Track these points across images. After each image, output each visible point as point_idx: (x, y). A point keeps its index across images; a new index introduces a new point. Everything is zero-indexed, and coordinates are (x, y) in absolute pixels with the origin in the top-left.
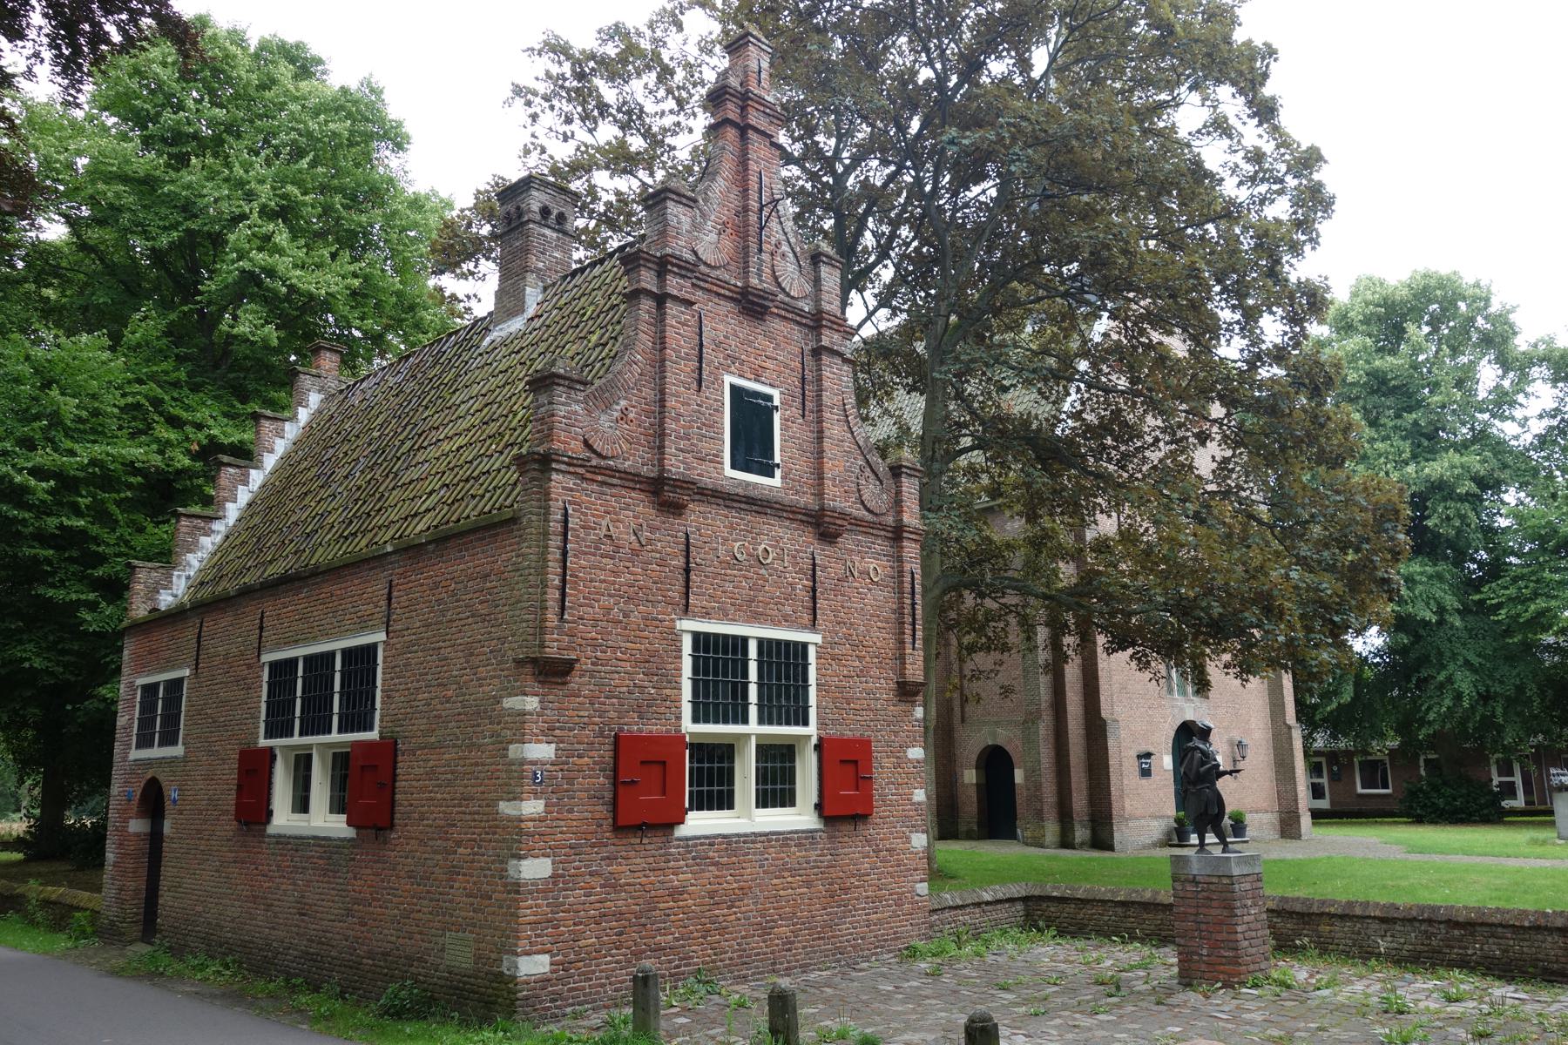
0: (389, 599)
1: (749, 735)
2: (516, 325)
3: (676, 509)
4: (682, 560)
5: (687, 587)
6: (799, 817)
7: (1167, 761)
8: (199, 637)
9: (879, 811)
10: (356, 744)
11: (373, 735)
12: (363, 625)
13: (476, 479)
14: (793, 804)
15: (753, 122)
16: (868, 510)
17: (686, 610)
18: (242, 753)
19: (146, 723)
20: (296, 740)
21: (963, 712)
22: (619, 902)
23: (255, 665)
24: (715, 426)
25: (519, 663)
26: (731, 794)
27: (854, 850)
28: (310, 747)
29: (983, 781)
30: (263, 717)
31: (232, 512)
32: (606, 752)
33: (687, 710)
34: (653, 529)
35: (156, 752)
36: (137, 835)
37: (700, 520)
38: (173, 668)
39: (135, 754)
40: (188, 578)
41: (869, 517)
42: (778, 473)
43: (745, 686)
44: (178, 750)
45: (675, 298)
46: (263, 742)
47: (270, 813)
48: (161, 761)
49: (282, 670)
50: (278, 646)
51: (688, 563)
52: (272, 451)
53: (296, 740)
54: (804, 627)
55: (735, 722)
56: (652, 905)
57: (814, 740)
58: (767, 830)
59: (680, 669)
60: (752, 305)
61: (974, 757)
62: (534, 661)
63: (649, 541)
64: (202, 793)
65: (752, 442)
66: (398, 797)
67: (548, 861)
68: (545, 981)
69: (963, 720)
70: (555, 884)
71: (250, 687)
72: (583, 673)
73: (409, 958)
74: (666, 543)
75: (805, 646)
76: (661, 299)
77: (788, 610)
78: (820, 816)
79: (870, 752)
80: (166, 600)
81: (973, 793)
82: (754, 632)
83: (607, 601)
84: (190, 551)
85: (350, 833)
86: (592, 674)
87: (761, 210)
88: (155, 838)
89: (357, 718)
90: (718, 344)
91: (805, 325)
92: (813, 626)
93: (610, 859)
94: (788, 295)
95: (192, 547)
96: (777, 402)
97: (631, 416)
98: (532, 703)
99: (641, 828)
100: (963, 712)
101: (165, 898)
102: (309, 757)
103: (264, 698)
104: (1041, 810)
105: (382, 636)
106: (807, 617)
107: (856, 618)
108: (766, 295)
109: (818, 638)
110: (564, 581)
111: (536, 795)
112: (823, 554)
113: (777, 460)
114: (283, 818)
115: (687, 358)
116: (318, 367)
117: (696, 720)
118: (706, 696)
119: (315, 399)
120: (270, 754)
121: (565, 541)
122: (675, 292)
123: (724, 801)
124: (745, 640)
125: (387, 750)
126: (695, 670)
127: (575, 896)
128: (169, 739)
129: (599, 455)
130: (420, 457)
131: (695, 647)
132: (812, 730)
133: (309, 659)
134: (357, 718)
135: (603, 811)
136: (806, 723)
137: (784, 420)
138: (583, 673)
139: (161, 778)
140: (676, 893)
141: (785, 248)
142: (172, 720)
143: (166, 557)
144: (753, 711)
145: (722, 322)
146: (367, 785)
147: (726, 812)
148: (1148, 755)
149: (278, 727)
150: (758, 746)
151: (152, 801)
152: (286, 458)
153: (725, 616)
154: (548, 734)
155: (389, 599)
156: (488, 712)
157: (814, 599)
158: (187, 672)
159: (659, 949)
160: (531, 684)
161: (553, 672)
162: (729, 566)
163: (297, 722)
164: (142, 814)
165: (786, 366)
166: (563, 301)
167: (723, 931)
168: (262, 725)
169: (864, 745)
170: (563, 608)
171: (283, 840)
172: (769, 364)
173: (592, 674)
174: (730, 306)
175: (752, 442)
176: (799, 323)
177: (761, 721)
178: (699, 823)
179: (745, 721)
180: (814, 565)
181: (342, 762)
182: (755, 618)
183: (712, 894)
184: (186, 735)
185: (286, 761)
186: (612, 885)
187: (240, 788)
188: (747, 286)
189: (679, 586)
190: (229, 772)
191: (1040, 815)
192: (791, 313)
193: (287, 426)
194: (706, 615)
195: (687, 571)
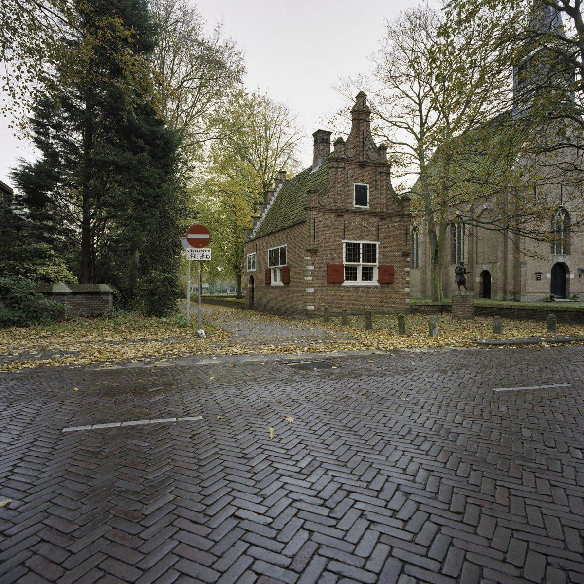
3: (342, 216)
6: (374, 282)
7: (549, 275)
11: (286, 265)
17: (344, 239)
20: (280, 266)
22: (329, 298)
26: (356, 277)
29: (482, 281)
33: (344, 260)
35: (252, 270)
42: (368, 205)
43: (359, 254)
44: (255, 270)
49: (271, 252)
50: (270, 248)
53: (274, 267)
57: (378, 266)
61: (479, 274)
62: (309, 250)
64: (259, 279)
65: (361, 198)
68: (313, 311)
79: (393, 269)
81: (479, 284)
82: (361, 242)
88: (253, 288)
92: (378, 240)
96: (368, 188)
98: (308, 258)
101: (255, 299)
106: (376, 238)
109: (379, 243)
111: (311, 276)
112: (380, 222)
113: (368, 201)
114: (273, 283)
124: (359, 244)
127: (319, 296)
132: (377, 263)
133: (275, 250)
134: (283, 263)
136: (375, 262)
141: (371, 148)
144: (361, 260)
145: (353, 171)
148: (540, 273)
149: (271, 264)
151: (252, 280)
153: (354, 239)
154: (313, 264)
156: (302, 260)
160: (309, 254)
161: (314, 252)
164: (250, 283)
172: (366, 178)
177: (363, 262)
178: (347, 283)
179: (359, 262)
181: (282, 270)
182: (362, 239)
188: (513, 90)
189: (342, 233)
190: (263, 274)
192: (372, 164)
194: (349, 239)
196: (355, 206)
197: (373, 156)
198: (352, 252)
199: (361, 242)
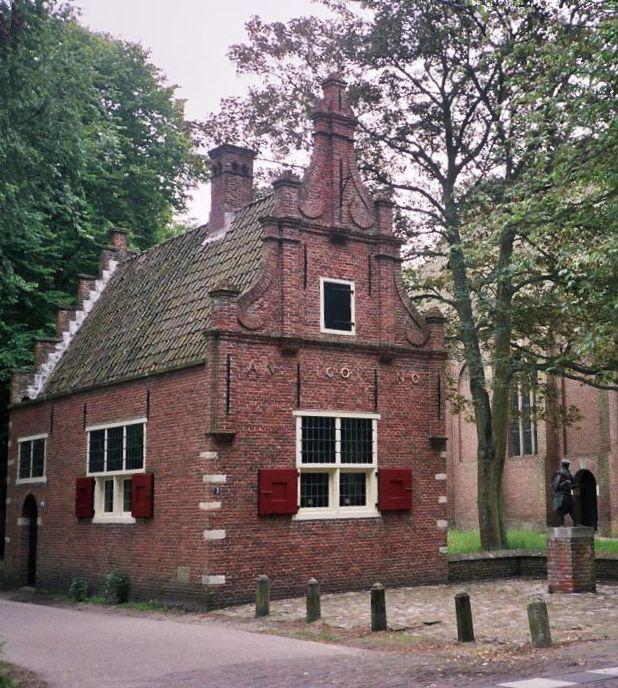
0: (148, 400)
1: (335, 469)
2: (221, 235)
4: (296, 379)
5: (299, 393)
6: (369, 510)
8: (52, 416)
9: (417, 508)
10: (134, 476)
11: (142, 471)
12: (136, 413)
13: (194, 333)
14: (327, 505)
15: (336, 130)
16: (413, 344)
17: (298, 406)
18: (78, 480)
19: (25, 463)
20: (105, 473)
21: (565, 448)
22: (264, 551)
23: (83, 433)
24: (314, 306)
25: (207, 435)
26: (327, 499)
27: (401, 531)
28: (112, 476)
30: (88, 461)
31: (67, 338)
32: (254, 478)
33: (299, 457)
34: (278, 364)
35: (31, 480)
36: (22, 526)
37: (309, 360)
38: (38, 432)
39: (20, 481)
40: (44, 378)
41: (413, 348)
42: (353, 328)
44: (43, 479)
45: (289, 241)
46: (89, 475)
47: (93, 512)
48: (33, 486)
49: (97, 436)
50: (94, 423)
51: (299, 380)
52: (88, 299)
53: (105, 473)
54: (371, 410)
55: (328, 461)
56: (280, 553)
57: (376, 471)
58: (346, 517)
59: (294, 436)
60: (338, 238)
63: (276, 370)
64: (59, 500)
65: (338, 314)
66: (155, 502)
67: (223, 531)
68: (222, 587)
69: (565, 454)
70: (228, 541)
71: (81, 444)
72: (241, 440)
73: (162, 581)
74: (286, 372)
75: (370, 421)
76: (281, 242)
77: (359, 401)
78: (379, 510)
80: (33, 392)
82: (338, 414)
83: (252, 403)
84: (44, 362)
85: (132, 520)
86: (245, 440)
87: (341, 182)
88: (33, 529)
89: (135, 462)
90: (316, 261)
91: (372, 243)
92: (375, 410)
93: (257, 531)
94: (360, 227)
95: (44, 360)
96: (353, 288)
97: (266, 306)
99: (272, 516)
100: (565, 448)
102: (112, 482)
103: (88, 451)
104: (609, 513)
105: (145, 420)
107: (403, 405)
108: (346, 231)
109: (378, 416)
110: (228, 395)
113: (353, 320)
114: (101, 516)
115: (297, 271)
116: (114, 244)
117: (304, 461)
118: (310, 449)
119: (113, 264)
120: (92, 480)
121: (229, 374)
122: (288, 237)
123: (323, 502)
124: (333, 419)
125: (150, 478)
126: (304, 436)
128: (39, 473)
129: (247, 329)
130: (167, 316)
131: (304, 424)
132: (374, 465)
134: (135, 462)
135: (253, 507)
136: (371, 461)
137: (357, 298)
138: (241, 440)
139: (34, 494)
140: (293, 548)
141: (358, 199)
142: (39, 462)
143: (33, 367)
144: (338, 457)
145: (318, 249)
146: (140, 497)
147: (326, 508)
149: (96, 466)
150: (341, 474)
151: (30, 508)
152: (97, 304)
153: (322, 407)
155: (148, 400)
156: (193, 458)
157: (376, 395)
158: (46, 435)
159: (284, 575)
162: (324, 381)
163: (124, 462)
165: (359, 268)
166: (244, 223)
167: (319, 567)
168: (88, 465)
169: (407, 474)
170: (228, 408)
171: (100, 526)
173: (245, 440)
174: (323, 238)
175: (338, 314)
176: (367, 243)
177: (343, 461)
178: (306, 514)
179: (334, 461)
180: (376, 377)
181: (129, 484)
182: (340, 407)
183: (313, 549)
184: (47, 471)
185: (101, 483)
186: (257, 543)
187: (77, 500)
191: (609, 517)
192: (361, 237)
193: (97, 282)
194: (310, 407)
195: (298, 385)
196: (323, 329)
197: (363, 218)
198: (318, 438)
199: (338, 414)
